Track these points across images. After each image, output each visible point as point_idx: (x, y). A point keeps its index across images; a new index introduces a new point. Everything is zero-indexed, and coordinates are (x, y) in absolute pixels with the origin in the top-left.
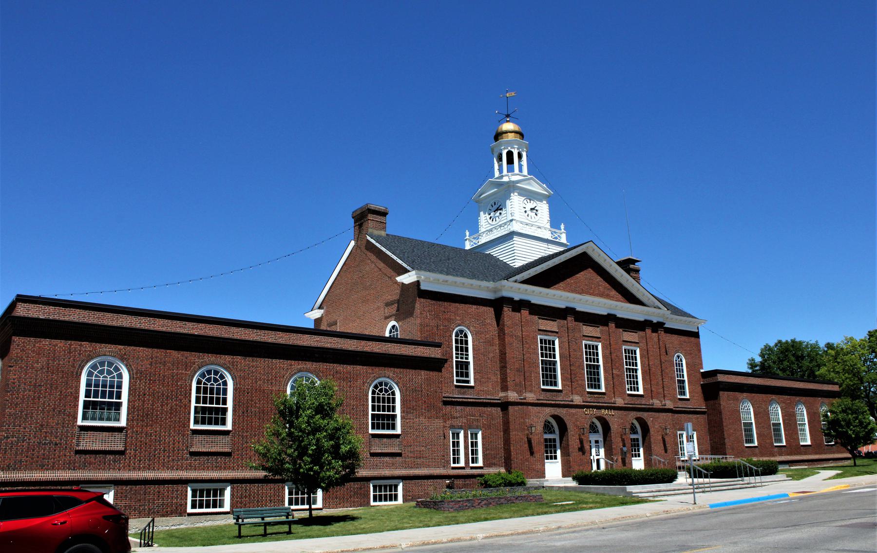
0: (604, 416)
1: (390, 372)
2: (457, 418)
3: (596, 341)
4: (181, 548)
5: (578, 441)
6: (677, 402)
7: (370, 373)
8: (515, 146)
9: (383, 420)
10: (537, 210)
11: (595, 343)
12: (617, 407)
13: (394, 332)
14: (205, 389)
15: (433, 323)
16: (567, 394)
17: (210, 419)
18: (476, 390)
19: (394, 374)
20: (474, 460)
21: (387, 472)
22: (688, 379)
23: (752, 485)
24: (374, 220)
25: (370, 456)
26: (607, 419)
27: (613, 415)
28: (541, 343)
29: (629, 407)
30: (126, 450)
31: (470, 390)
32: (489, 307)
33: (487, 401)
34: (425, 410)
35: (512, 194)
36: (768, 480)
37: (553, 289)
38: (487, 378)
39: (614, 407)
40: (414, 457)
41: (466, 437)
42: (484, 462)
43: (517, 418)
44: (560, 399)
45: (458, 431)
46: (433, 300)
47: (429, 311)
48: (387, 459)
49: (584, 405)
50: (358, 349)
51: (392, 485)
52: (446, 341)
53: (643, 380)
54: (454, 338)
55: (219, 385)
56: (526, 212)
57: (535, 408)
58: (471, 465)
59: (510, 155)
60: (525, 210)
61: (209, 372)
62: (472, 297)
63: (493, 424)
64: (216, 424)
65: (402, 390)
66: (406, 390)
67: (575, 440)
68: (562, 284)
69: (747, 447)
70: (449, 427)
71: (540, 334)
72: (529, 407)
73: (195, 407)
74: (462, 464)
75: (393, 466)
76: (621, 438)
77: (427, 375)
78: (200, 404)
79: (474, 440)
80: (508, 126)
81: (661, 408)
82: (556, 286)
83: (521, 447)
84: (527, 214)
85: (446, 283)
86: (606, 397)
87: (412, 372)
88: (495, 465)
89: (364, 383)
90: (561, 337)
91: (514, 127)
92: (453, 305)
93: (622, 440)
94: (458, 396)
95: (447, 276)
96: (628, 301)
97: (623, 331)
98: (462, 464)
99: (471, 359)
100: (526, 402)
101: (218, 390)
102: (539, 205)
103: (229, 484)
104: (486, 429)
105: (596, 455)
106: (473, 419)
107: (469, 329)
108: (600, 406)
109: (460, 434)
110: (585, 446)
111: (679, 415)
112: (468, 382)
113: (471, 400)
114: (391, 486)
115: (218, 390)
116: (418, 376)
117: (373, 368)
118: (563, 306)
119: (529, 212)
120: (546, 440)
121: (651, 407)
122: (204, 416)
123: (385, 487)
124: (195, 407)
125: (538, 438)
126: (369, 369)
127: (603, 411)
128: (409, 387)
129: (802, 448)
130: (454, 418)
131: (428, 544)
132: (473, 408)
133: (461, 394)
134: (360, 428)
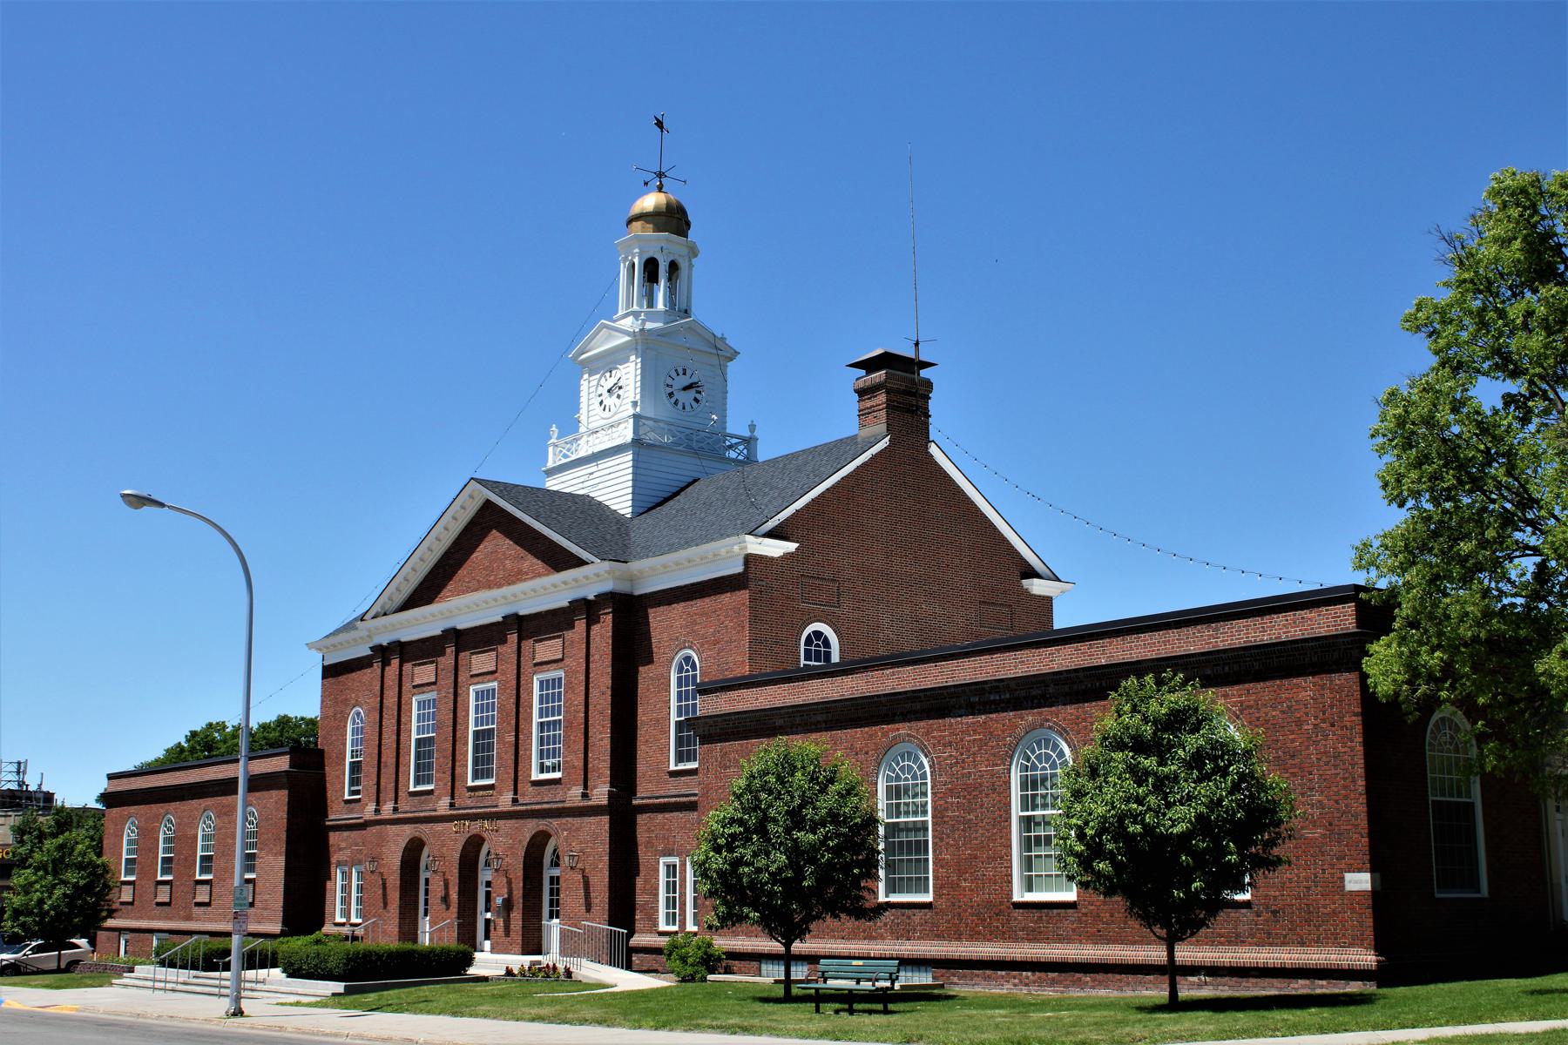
5: (442, 883)
6: (666, 783)
13: (687, 671)
23: (169, 986)
29: (520, 811)
36: (300, 991)
49: (451, 815)
54: (802, 647)
56: (671, 394)
60: (669, 390)
68: (445, 592)
84: (681, 372)
93: (507, 882)
108: (474, 814)
110: (451, 893)
111: (667, 815)
121: (560, 805)
127: (479, 823)
129: (1017, 913)
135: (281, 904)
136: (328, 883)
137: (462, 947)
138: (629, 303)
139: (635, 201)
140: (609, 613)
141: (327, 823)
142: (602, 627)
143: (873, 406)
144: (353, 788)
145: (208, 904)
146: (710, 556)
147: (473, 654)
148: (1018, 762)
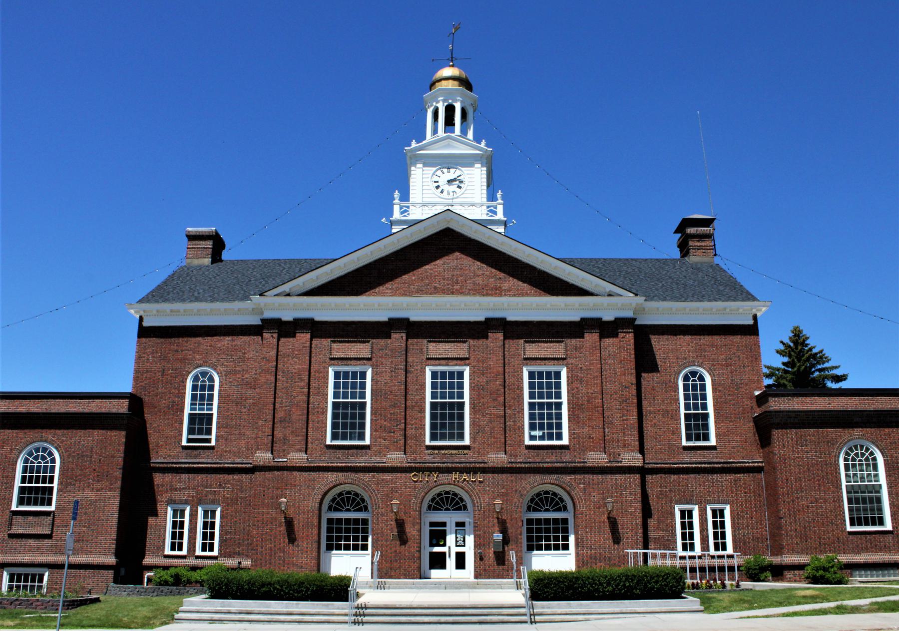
1: (49, 434)
2: (180, 490)
3: (460, 365)
7: (21, 438)
8: (459, 98)
9: (37, 493)
10: (461, 182)
11: (552, 368)
12: (489, 468)
14: (32, 468)
15: (157, 367)
17: (29, 499)
19: (54, 437)
21: (27, 558)
22: (715, 410)
24: (195, 248)
25: (9, 537)
30: (52, 533)
31: (206, 451)
32: (254, 335)
33: (235, 466)
34: (93, 481)
35: (413, 168)
37: (369, 295)
38: (239, 434)
39: (484, 468)
42: (188, 551)
43: (268, 489)
45: (181, 507)
46: (161, 338)
47: (152, 353)
48: (31, 542)
49: (411, 468)
50: (10, 411)
51: (21, 574)
52: (175, 389)
55: (47, 462)
57: (306, 474)
58: (199, 552)
59: (450, 110)
60: (437, 184)
61: (37, 450)
62: (225, 325)
63: (241, 498)
64: (42, 504)
65: (63, 456)
66: (69, 457)
67: (387, 521)
68: (389, 285)
70: (166, 502)
71: (334, 365)
72: (293, 473)
73: (846, 485)
74: (698, 551)
75: (39, 550)
76: (498, 518)
77: (102, 436)
78: (39, 483)
79: (209, 520)
80: (447, 72)
81: (607, 467)
82: (377, 290)
83: (271, 530)
84: (440, 190)
85: (724, 312)
86: (470, 452)
87: (81, 433)
88: (239, 555)
89: (11, 450)
90: (377, 365)
91: (460, 71)
92: (193, 340)
94: (186, 461)
95: (212, 304)
96: (549, 294)
97: (526, 342)
99: (215, 411)
101: (46, 468)
102: (466, 172)
103: (46, 569)
104: (227, 504)
105: (457, 546)
106: (206, 491)
107: (215, 369)
109: (725, 511)
112: (209, 441)
113: (204, 465)
114: (34, 576)
115: (46, 468)
116: (89, 437)
117: (26, 431)
118: (577, 319)
119: (447, 188)
120: (529, 521)
122: (26, 496)
123: (26, 576)
124: (846, 485)
125: (308, 519)
126: (21, 433)
128: (74, 452)
130: (176, 490)
132: (209, 476)
133: (191, 457)
135: (114, 535)
136: (151, 520)
137: (525, 581)
138: (435, 131)
139: (436, 72)
140: (631, 332)
141: (152, 465)
142: (620, 341)
143: (702, 246)
144: (191, 437)
145: (49, 537)
146: (182, 311)
147: (430, 342)
148: (24, 455)
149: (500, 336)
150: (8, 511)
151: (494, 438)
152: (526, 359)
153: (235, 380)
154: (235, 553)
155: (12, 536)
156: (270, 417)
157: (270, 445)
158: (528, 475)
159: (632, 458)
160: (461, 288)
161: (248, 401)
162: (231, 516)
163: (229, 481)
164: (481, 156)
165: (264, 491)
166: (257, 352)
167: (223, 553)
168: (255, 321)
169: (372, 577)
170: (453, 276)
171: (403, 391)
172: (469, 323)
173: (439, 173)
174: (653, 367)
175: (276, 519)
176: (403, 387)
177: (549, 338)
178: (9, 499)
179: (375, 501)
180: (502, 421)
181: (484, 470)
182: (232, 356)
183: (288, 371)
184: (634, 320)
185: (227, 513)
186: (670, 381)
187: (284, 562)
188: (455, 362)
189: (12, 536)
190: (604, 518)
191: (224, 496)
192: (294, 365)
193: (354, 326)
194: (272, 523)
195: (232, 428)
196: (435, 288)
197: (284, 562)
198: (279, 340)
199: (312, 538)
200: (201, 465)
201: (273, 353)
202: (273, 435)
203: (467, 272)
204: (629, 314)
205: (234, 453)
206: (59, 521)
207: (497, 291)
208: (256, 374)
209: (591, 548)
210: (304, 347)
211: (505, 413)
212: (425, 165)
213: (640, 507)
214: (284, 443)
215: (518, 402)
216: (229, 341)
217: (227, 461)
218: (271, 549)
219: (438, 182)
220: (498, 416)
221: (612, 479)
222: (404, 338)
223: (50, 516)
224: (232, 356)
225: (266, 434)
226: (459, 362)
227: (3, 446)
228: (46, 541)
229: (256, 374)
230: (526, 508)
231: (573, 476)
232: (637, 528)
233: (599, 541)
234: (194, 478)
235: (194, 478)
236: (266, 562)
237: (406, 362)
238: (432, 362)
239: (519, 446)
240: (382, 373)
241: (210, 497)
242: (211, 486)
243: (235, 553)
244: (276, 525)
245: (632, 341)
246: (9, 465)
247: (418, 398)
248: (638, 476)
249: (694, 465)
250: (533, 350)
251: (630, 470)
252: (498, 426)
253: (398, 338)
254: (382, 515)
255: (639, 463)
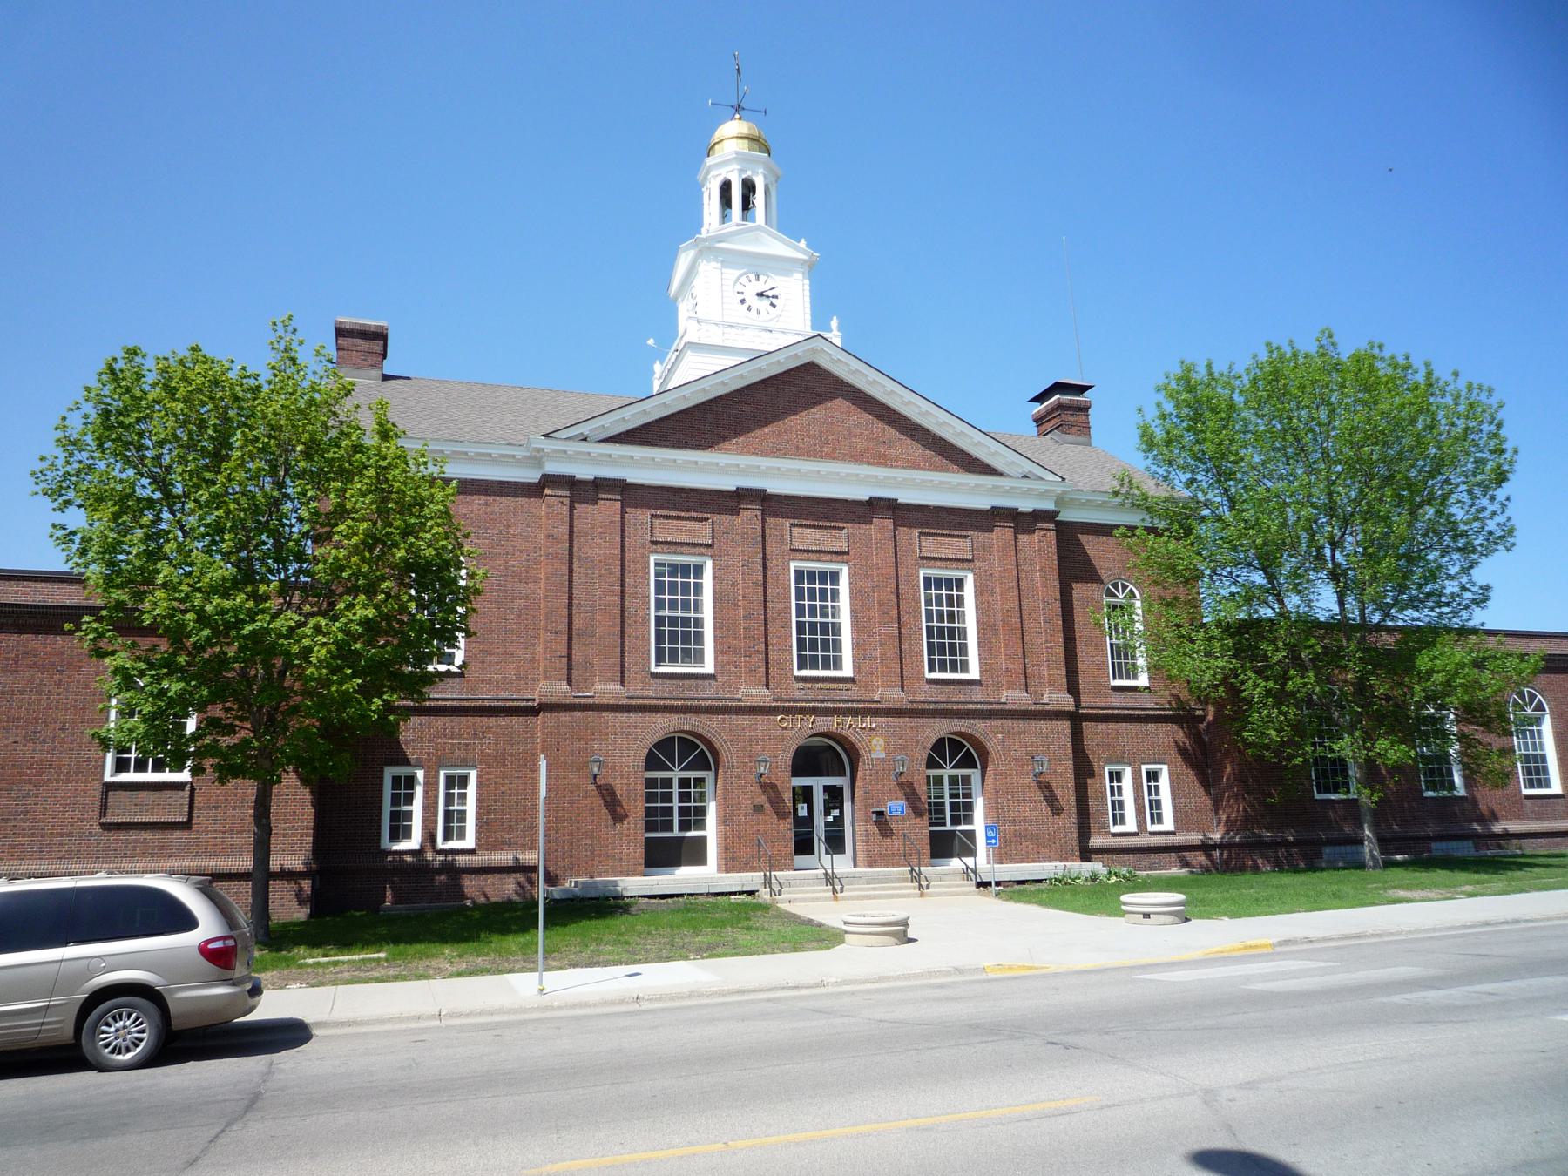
0: (844, 733)
4: (424, 982)
16: (728, 685)
18: (468, 681)
20: (1157, 818)
26: (852, 739)
27: (874, 729)
28: (927, 587)
33: (500, 704)
38: (505, 653)
40: (224, 833)
41: (431, 785)
43: (565, 740)
44: (708, 694)
48: (147, 836)
53: (979, 646)
56: (743, 301)
57: (623, 717)
58: (1151, 828)
60: (741, 297)
69: (1529, 797)
71: (656, 552)
83: (572, 804)
84: (746, 305)
88: (510, 845)
91: (749, 129)
98: (1131, 825)
100: (594, 704)
120: (651, 783)
131: (459, 1015)
134: (78, 771)
145: (186, 826)
149: (889, 523)
150: (96, 782)
151: (887, 668)
152: (922, 558)
153: (493, 568)
154: (503, 843)
155: (107, 827)
156: (563, 628)
157: (565, 671)
158: (932, 720)
159: (1058, 697)
160: (833, 452)
161: (518, 602)
162: (496, 783)
163: (489, 728)
164: (804, 261)
165: (558, 743)
166: (528, 526)
167: (484, 843)
168: (533, 476)
169: (989, 863)
170: (821, 432)
171: (761, 595)
172: (846, 501)
173: (744, 280)
174: (1091, 575)
175: (578, 787)
176: (761, 590)
177: (675, 509)
178: (96, 761)
179: (727, 757)
180: (896, 643)
181: (876, 713)
182: (487, 529)
183: (587, 558)
184: (1057, 513)
185: (489, 780)
186: (1093, 599)
187: (592, 852)
188: (828, 557)
189: (107, 827)
190: (1029, 779)
191: (482, 752)
192: (597, 549)
193: (684, 495)
194: (572, 793)
195: (491, 644)
196: (797, 448)
197: (592, 852)
198: (572, 508)
199: (636, 813)
200: (443, 703)
201: (565, 529)
202: (569, 656)
203: (840, 429)
204: (1049, 505)
205: (497, 683)
206: (200, 799)
207: (881, 460)
208: (528, 561)
209: (1014, 823)
210: (611, 522)
211: (900, 634)
212: (724, 264)
213: (1072, 766)
214: (586, 669)
215: (914, 617)
216: (479, 504)
217: (486, 695)
218: (571, 834)
219: (742, 293)
220: (891, 637)
221: (1036, 728)
222: (760, 517)
223: (183, 790)
224: (487, 529)
225: (559, 654)
226: (834, 557)
227: (80, 667)
228: (178, 833)
229: (528, 561)
230: (924, 762)
231: (988, 723)
232: (1069, 794)
233: (1025, 812)
234: (429, 724)
235: (429, 724)
236: (564, 854)
237: (764, 554)
238: (799, 555)
239: (918, 680)
240: (727, 567)
241: (458, 753)
242: (460, 736)
243: (503, 843)
244: (579, 796)
245: (1054, 542)
246: (94, 701)
247: (780, 606)
248: (1067, 724)
249: (1126, 712)
250: (932, 547)
251: (1057, 715)
252: (893, 652)
253: (749, 518)
254: (738, 777)
255: (1071, 707)
